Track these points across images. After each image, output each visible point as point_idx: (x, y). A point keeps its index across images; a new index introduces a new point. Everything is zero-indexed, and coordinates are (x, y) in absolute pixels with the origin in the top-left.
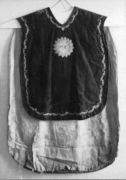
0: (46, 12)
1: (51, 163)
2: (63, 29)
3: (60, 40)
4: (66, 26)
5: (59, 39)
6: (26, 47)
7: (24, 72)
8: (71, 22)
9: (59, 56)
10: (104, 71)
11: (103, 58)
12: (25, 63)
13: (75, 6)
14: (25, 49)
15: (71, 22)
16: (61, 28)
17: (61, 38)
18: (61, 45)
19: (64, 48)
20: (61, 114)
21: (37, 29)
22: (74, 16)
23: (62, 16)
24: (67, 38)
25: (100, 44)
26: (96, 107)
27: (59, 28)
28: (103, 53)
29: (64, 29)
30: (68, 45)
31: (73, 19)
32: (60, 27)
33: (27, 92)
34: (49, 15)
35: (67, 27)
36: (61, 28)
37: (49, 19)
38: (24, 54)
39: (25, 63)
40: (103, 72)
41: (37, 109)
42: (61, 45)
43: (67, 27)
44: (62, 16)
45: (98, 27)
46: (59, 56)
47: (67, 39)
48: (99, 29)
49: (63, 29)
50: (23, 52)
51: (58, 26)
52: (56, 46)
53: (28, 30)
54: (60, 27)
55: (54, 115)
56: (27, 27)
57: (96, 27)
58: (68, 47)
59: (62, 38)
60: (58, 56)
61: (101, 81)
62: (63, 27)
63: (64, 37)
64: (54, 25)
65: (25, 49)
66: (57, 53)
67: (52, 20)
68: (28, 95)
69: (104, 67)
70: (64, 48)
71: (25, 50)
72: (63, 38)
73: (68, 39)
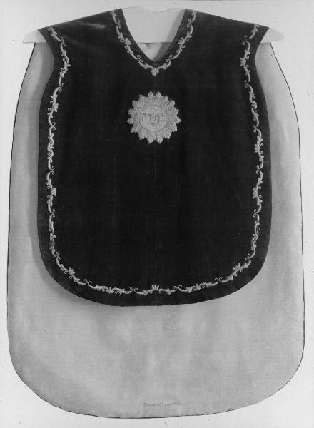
0: (117, 27)
1: (147, 173)
2: (155, 72)
3: (146, 98)
4: (162, 65)
5: (142, 97)
6: (56, 107)
7: (48, 171)
8: (176, 56)
9: (141, 139)
10: (261, 173)
11: (256, 140)
12: (50, 147)
13: (185, 8)
14: (54, 112)
15: (176, 56)
16: (149, 70)
17: (149, 94)
18: (147, 111)
19: (154, 119)
20: (139, 291)
21: (87, 65)
22: (182, 41)
23: (151, 32)
24: (164, 95)
25: (249, 105)
26: (242, 268)
27: (146, 68)
28: (258, 125)
29: (158, 71)
30: (164, 112)
31: (181, 46)
32: (146, 66)
33: (51, 224)
34: (124, 36)
35: (165, 67)
36: (149, 70)
37: (124, 44)
38: (51, 124)
39: (50, 147)
40: (259, 176)
41: (75, 271)
42: (147, 111)
43: (165, 67)
44: (151, 32)
45: (244, 61)
46: (141, 139)
47: (163, 99)
48: (245, 67)
49: (155, 72)
50: (49, 119)
51: (144, 63)
52: (136, 115)
53: (66, 65)
54: (146, 66)
55: (121, 293)
56: (64, 57)
57: (239, 62)
58: (164, 119)
59: (151, 94)
60: (138, 138)
61: (256, 199)
62: (156, 67)
63: (156, 92)
64: (135, 60)
65: (54, 112)
66: (137, 131)
67: (74, 277)
68: (54, 231)
69: (257, 207)
70: (154, 119)
71: (53, 114)
72: (154, 94)
73: (166, 97)
